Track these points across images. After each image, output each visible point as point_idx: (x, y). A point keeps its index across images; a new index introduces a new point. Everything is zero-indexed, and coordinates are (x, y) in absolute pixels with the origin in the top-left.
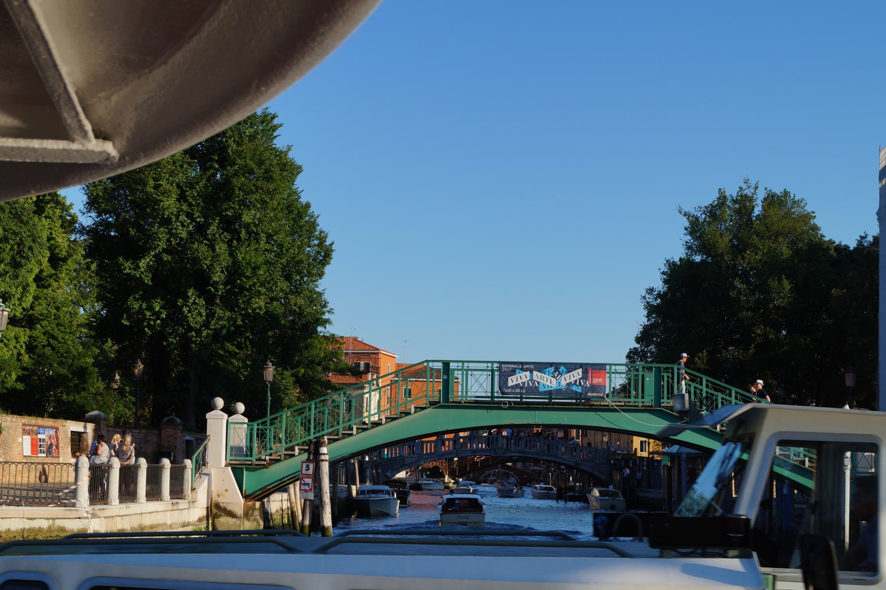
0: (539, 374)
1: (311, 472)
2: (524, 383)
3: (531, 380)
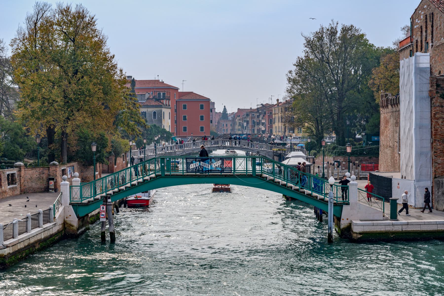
0: (203, 163)
1: (104, 210)
2: (196, 167)
3: (200, 166)
